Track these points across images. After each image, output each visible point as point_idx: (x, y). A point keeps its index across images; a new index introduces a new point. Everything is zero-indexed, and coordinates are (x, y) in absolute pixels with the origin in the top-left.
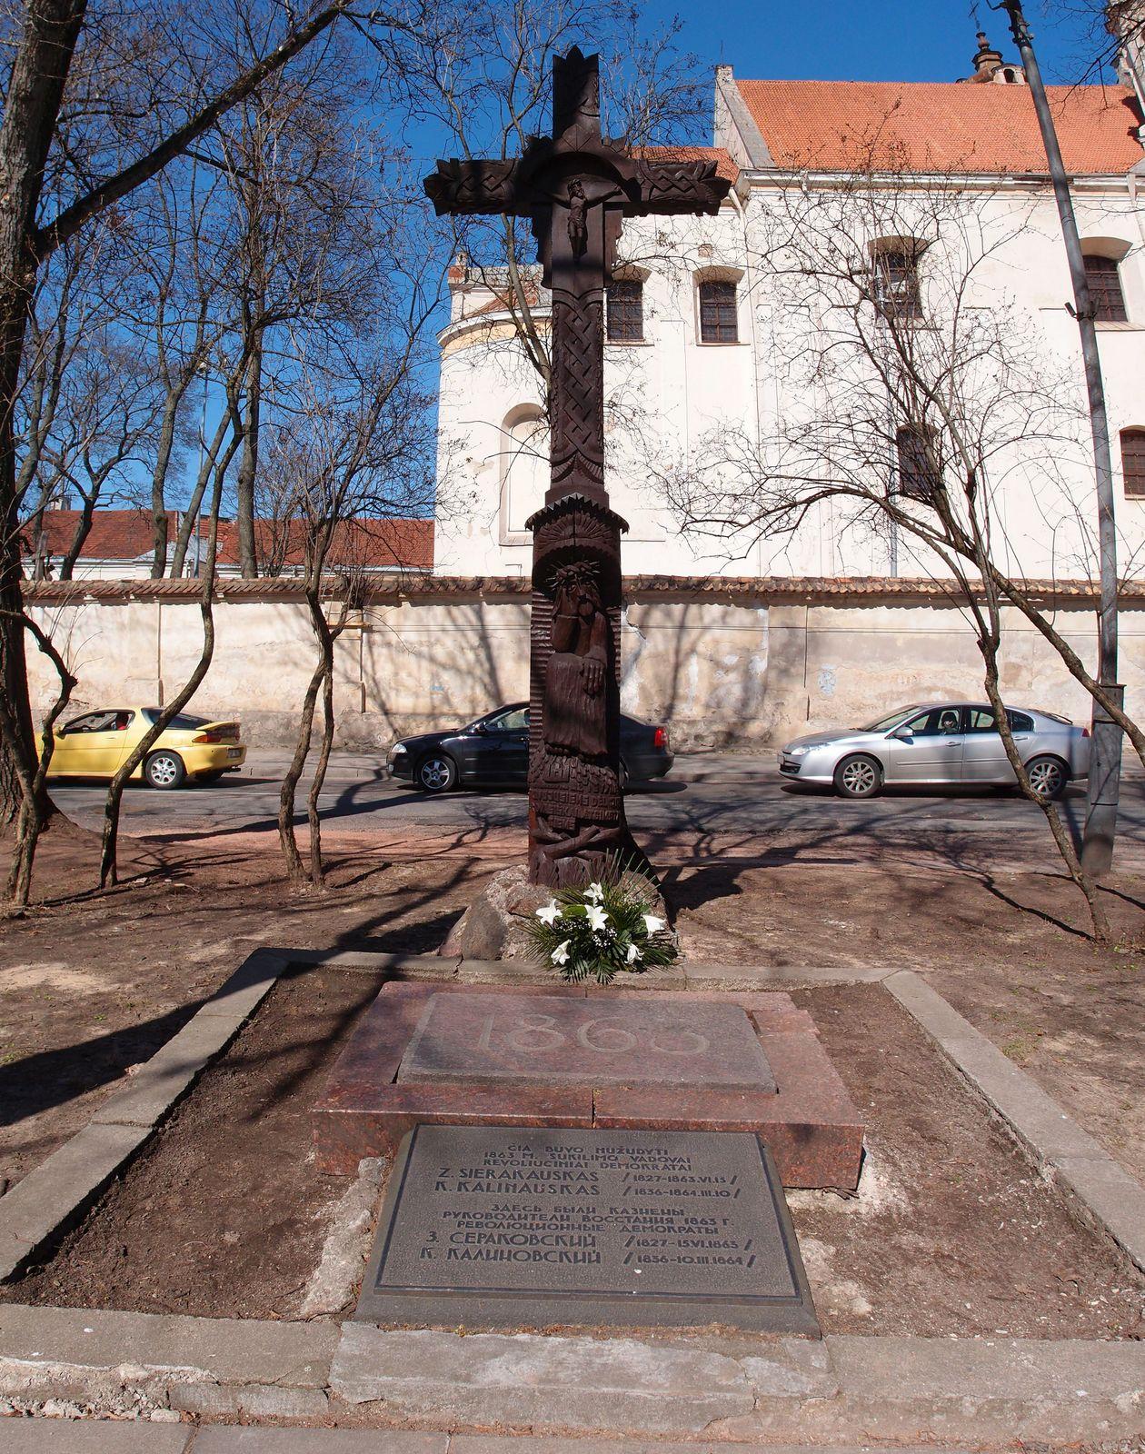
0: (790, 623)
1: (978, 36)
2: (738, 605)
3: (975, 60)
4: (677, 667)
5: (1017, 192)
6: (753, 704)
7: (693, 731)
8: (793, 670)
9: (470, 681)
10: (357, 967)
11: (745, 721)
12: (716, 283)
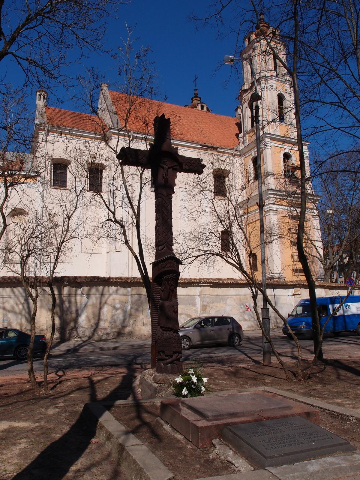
0: (138, 293)
1: (195, 90)
2: (121, 287)
3: (193, 98)
4: (100, 309)
5: (200, 150)
6: (127, 320)
7: (105, 332)
8: (139, 309)
9: (20, 317)
10: (124, 404)
11: (124, 327)
12: (61, 165)
